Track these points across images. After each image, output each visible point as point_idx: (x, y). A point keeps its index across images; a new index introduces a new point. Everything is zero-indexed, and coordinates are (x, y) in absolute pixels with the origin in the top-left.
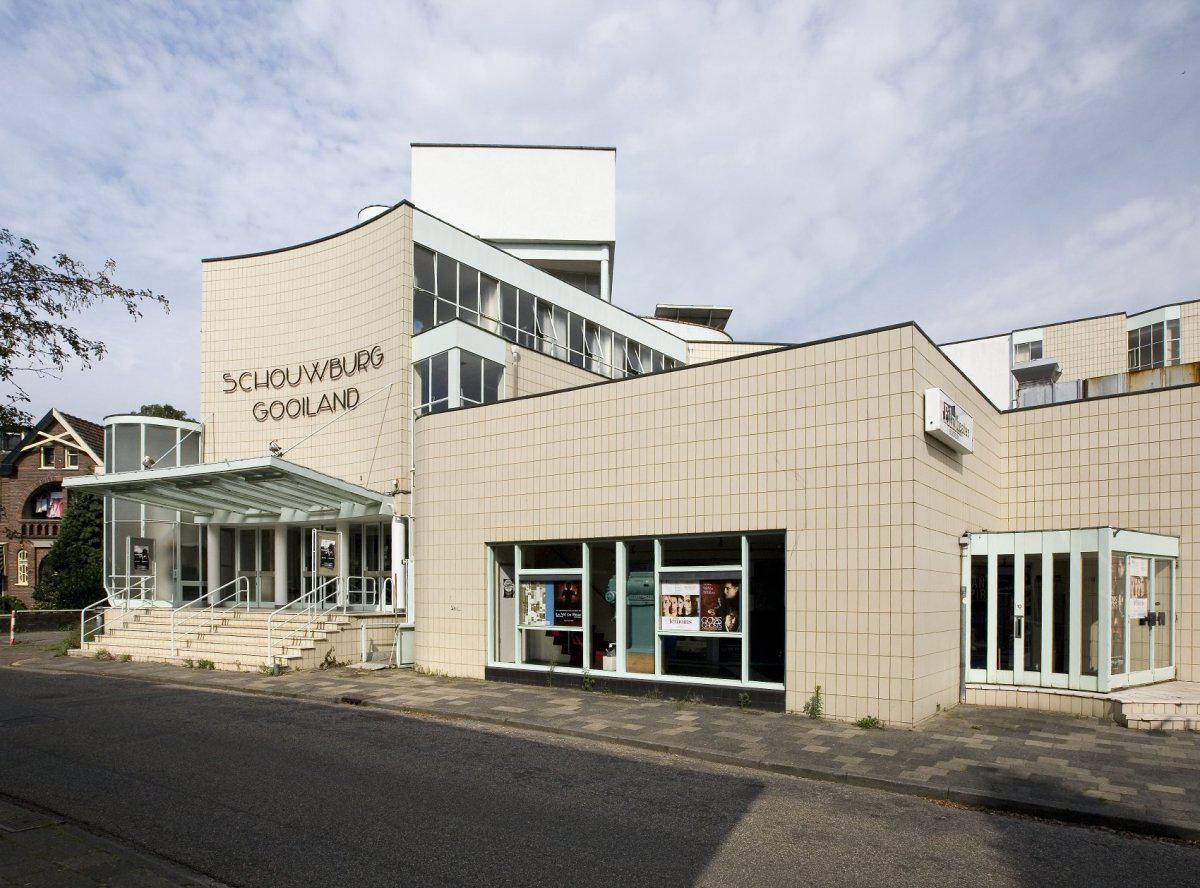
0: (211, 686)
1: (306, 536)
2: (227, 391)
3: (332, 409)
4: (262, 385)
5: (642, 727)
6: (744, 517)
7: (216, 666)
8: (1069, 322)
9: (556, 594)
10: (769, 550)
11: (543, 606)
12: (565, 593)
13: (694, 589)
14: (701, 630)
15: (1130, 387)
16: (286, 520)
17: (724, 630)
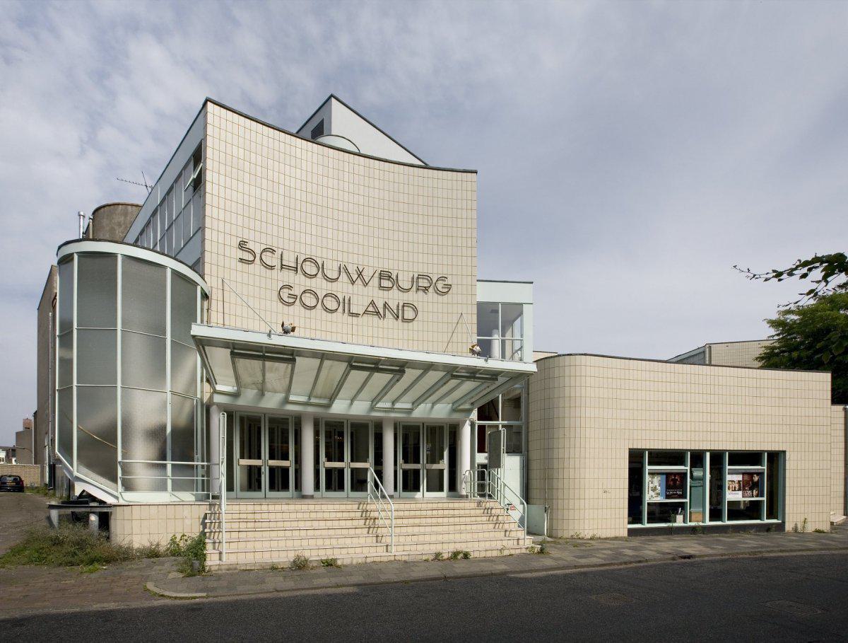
1: (450, 433)
2: (241, 260)
4: (289, 268)
6: (720, 443)
7: (472, 556)
8: (630, 359)
9: (667, 481)
10: (776, 458)
12: (672, 480)
13: (740, 477)
14: (743, 497)
15: (331, 366)
17: (753, 497)
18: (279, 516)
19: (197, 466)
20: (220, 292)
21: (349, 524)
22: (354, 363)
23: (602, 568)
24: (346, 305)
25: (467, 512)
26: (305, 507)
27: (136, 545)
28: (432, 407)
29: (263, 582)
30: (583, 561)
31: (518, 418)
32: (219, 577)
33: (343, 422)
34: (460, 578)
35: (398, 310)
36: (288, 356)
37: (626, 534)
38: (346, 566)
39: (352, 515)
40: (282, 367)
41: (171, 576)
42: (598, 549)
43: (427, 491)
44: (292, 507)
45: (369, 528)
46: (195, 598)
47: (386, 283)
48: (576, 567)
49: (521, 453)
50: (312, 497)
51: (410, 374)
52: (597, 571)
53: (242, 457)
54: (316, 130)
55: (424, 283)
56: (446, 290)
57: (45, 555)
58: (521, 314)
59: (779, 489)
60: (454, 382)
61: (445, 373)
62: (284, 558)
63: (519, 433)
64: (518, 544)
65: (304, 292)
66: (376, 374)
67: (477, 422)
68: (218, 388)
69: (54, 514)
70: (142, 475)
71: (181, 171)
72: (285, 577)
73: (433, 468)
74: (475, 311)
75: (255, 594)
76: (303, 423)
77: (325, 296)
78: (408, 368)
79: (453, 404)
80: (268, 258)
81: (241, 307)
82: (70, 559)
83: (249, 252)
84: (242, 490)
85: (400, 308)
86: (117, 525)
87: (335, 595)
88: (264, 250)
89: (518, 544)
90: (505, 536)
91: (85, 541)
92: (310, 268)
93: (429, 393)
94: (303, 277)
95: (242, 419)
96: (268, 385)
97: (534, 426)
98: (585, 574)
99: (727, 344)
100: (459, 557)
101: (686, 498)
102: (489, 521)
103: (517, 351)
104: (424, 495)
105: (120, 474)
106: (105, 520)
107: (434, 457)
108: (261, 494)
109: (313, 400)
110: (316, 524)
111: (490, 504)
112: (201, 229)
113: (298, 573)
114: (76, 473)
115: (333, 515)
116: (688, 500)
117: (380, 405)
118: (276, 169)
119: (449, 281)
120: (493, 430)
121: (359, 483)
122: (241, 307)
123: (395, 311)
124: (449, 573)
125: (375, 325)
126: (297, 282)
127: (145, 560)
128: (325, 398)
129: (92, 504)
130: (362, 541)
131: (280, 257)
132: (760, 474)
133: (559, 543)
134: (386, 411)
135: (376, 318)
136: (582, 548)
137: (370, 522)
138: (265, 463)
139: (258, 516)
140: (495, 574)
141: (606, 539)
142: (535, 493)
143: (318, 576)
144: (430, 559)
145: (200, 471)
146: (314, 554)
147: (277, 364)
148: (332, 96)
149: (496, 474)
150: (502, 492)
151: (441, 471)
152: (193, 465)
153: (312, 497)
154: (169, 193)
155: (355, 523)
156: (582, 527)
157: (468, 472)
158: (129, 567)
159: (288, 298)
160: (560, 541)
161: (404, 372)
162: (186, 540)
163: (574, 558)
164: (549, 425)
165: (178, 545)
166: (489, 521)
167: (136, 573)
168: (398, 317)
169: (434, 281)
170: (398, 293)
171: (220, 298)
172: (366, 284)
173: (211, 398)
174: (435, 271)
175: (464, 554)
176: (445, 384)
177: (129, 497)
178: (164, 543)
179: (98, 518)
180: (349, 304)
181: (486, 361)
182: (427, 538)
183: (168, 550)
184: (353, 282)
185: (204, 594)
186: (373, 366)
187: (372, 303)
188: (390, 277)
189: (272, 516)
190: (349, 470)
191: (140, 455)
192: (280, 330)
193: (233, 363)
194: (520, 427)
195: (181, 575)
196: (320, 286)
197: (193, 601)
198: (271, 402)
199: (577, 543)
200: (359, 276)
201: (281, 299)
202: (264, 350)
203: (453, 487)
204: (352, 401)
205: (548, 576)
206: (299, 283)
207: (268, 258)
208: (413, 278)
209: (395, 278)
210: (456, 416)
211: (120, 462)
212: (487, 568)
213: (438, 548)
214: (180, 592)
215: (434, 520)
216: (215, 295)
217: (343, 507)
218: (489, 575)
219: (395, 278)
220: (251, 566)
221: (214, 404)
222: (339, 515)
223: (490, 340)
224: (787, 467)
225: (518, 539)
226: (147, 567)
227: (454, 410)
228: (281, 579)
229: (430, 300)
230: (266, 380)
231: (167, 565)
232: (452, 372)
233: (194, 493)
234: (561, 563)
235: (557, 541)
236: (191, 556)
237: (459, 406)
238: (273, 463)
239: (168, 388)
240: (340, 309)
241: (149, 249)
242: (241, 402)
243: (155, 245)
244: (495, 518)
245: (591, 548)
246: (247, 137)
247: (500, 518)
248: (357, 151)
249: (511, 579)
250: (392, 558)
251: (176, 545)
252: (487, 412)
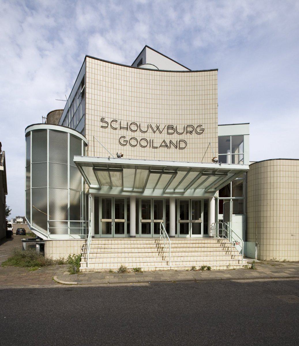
1: (204, 204)
2: (102, 127)
4: (124, 128)
18: (116, 246)
19: (81, 222)
20: (93, 142)
21: (150, 250)
22: (152, 169)
23: (287, 279)
24: (151, 143)
25: (212, 245)
26: (132, 242)
27: (54, 259)
28: (195, 191)
29: (104, 278)
30: (276, 275)
31: (241, 195)
32: (85, 275)
33: (150, 200)
34: (203, 280)
35: (177, 143)
36: (119, 168)
38: (145, 272)
39: (151, 246)
40: (118, 174)
41: (65, 273)
42: (287, 268)
44: (123, 242)
45: (159, 252)
46: (72, 284)
47: (170, 131)
48: (271, 278)
49: (243, 214)
50: (135, 237)
51: (180, 175)
52: (284, 281)
53: (103, 218)
54: (139, 62)
55: (190, 129)
56: (201, 132)
57: (18, 262)
58: (243, 141)
60: (203, 177)
61: (199, 173)
62: (115, 267)
63: (242, 204)
64: (239, 263)
65: (131, 139)
66: (163, 175)
67: (218, 198)
68: (91, 186)
69: (24, 244)
70: (59, 227)
71: (77, 91)
72: (115, 276)
74: (217, 141)
75: (99, 284)
76: (131, 201)
77: (141, 140)
78: (179, 171)
79: (205, 189)
80: (114, 125)
81: (102, 147)
82: (27, 264)
84: (103, 233)
85: (178, 142)
86: (47, 250)
87: (136, 287)
88: (113, 121)
89: (239, 263)
90: (232, 258)
91: (34, 256)
92: (134, 127)
93: (192, 184)
94: (132, 132)
95: (103, 201)
96: (114, 184)
97: (250, 199)
98: (276, 282)
100: (205, 269)
103: (241, 160)
104: (191, 236)
105: (48, 227)
106: (42, 247)
107: (196, 216)
108: (111, 236)
109: (135, 190)
110: (133, 250)
111: (225, 241)
112: (84, 115)
113: (121, 274)
114: (31, 227)
115: (142, 246)
117: (167, 191)
118: (118, 83)
120: (226, 202)
121: (157, 231)
122: (102, 147)
123: (176, 144)
124: (197, 278)
125: (166, 152)
126: (128, 134)
127: (57, 265)
128: (141, 188)
129: (37, 240)
130: (155, 259)
131: (119, 124)
133: (263, 264)
134: (171, 194)
135: (166, 148)
136: (277, 267)
137: (160, 249)
138: (113, 220)
139: (106, 246)
140: (223, 280)
141: (293, 262)
142: (251, 236)
143: (130, 276)
144: (189, 270)
145: (83, 225)
146: (130, 266)
147: (115, 173)
148: (146, 46)
149: (229, 226)
150: (231, 235)
151: (200, 224)
152: (80, 222)
153: (135, 237)
154: (73, 101)
155: (153, 250)
156: (278, 255)
157: (213, 224)
158: (50, 268)
159: (123, 142)
160: (264, 262)
161: (177, 173)
162: (75, 257)
163: (271, 273)
164: (259, 199)
165: (72, 259)
167: (51, 271)
168: (177, 147)
169: (195, 128)
170: (177, 135)
171: (93, 145)
172: (161, 132)
173: (88, 191)
174: (196, 123)
175: (208, 268)
176: (199, 178)
177: (53, 237)
178: (66, 258)
179: (39, 246)
180: (153, 143)
181: (220, 165)
182: (189, 259)
183: (67, 261)
184: (154, 132)
185: (76, 283)
186: (161, 171)
187: (164, 141)
188: (173, 128)
189: (113, 246)
190: (153, 223)
191: (59, 217)
192: (116, 156)
193: (95, 173)
194: (242, 200)
195: (69, 273)
196: (138, 135)
197: (71, 286)
198: (115, 191)
199: (274, 264)
200: (157, 129)
201: (120, 143)
202: (107, 166)
203: (206, 232)
204: (154, 189)
205: (253, 283)
206: (129, 135)
207: (114, 125)
208: (184, 127)
209: (175, 128)
210: (207, 195)
211: (48, 221)
212: (219, 276)
213: (194, 264)
214: (67, 281)
215: (194, 249)
216: (90, 144)
217: (148, 242)
218: (220, 280)
219: (175, 128)
220: (100, 270)
221: (90, 193)
222: (145, 246)
223: (226, 155)
225: (239, 261)
226: (56, 269)
227: (206, 192)
228: (113, 277)
229: (193, 137)
230: (112, 181)
231: (65, 269)
232: (204, 172)
233: (80, 235)
234: (263, 275)
235: (263, 262)
236: (74, 264)
237: (208, 190)
238: (117, 220)
239: (69, 187)
240: (148, 146)
241: (66, 127)
242: (102, 192)
243: (68, 125)
244: (227, 248)
245: (283, 267)
246: (104, 70)
247: (230, 249)
248: (156, 69)
250: (169, 269)
251: (71, 259)
252: (224, 192)
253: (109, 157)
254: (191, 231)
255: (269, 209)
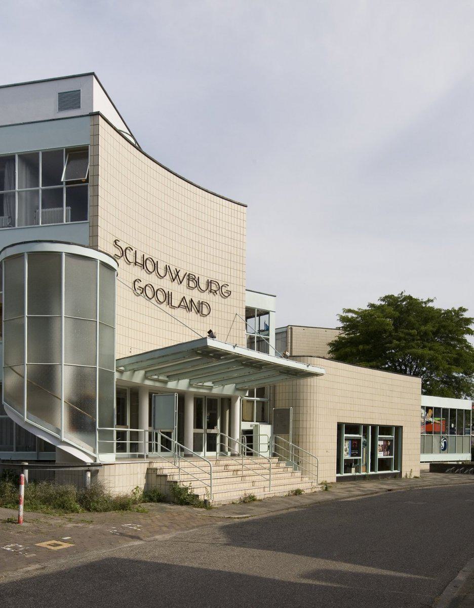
0: (353, 497)
3: (189, 309)
5: (38, 545)
9: (352, 445)
10: (399, 429)
11: (348, 449)
16: (215, 392)
37: (334, 480)
43: (207, 451)
47: (192, 284)
59: (399, 449)
73: (212, 432)
83: (118, 249)
99: (304, 328)
101: (360, 456)
102: (284, 471)
116: (361, 458)
119: (229, 288)
132: (391, 441)
166: (284, 471)
224: (403, 437)
249: (341, 502)
253: (236, 345)
254: (205, 447)
255: (308, 419)
